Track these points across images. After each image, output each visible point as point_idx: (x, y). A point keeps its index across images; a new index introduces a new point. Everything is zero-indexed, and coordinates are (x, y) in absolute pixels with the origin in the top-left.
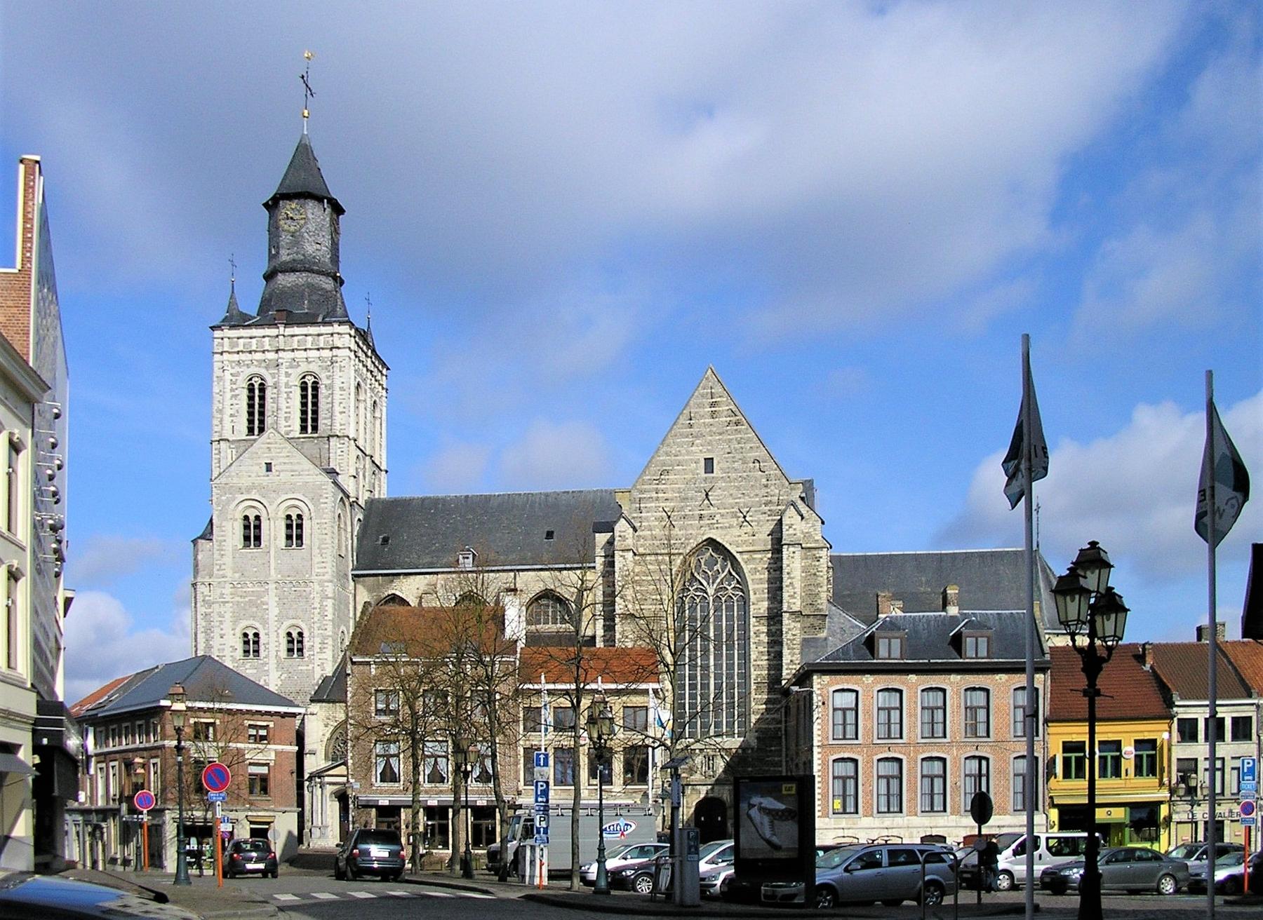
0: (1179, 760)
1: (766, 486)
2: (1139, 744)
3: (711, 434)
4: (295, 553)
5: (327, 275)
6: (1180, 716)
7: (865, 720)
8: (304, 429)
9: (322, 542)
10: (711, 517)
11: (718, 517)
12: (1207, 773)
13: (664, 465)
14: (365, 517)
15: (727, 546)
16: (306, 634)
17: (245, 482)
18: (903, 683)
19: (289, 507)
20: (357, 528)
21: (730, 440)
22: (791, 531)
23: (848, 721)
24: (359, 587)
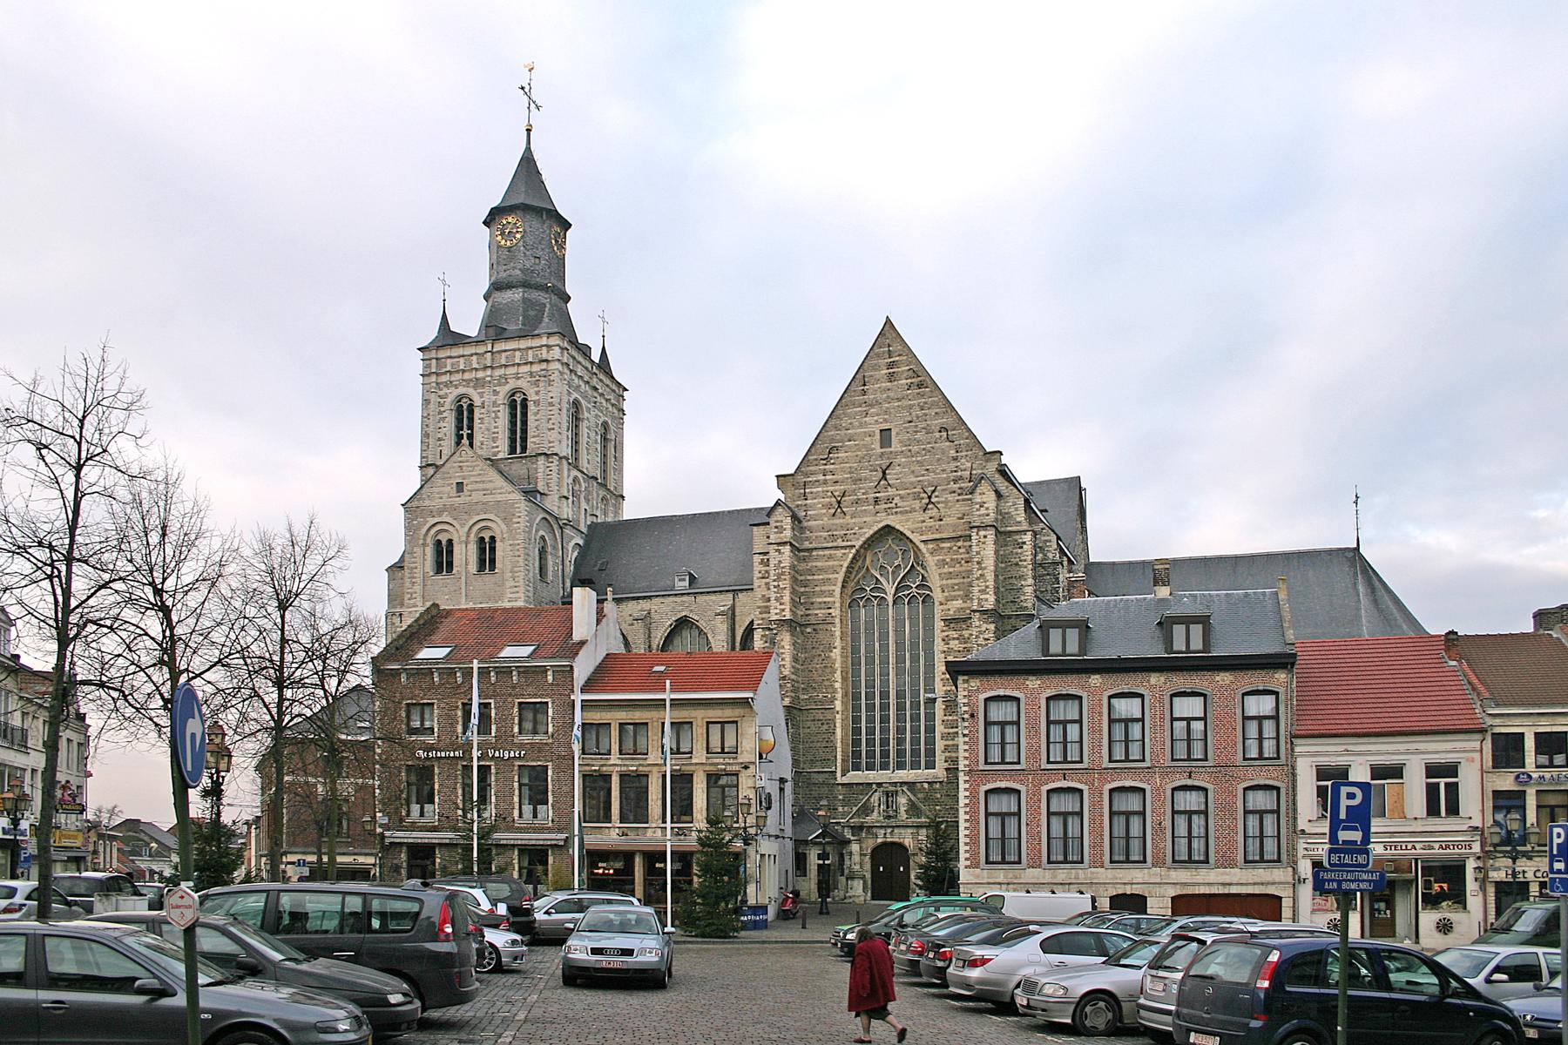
0: (1494, 792)
1: (955, 459)
2: (1433, 771)
3: (889, 400)
4: (488, 578)
5: (545, 288)
6: (1497, 730)
7: (1028, 737)
8: (513, 450)
9: (515, 564)
10: (889, 500)
11: (897, 500)
12: (577, 636)
13: (832, 440)
14: (587, 543)
15: (908, 533)
17: (437, 503)
18: (1083, 687)
19: (482, 529)
21: (911, 407)
22: (983, 511)
23: (1059, 747)
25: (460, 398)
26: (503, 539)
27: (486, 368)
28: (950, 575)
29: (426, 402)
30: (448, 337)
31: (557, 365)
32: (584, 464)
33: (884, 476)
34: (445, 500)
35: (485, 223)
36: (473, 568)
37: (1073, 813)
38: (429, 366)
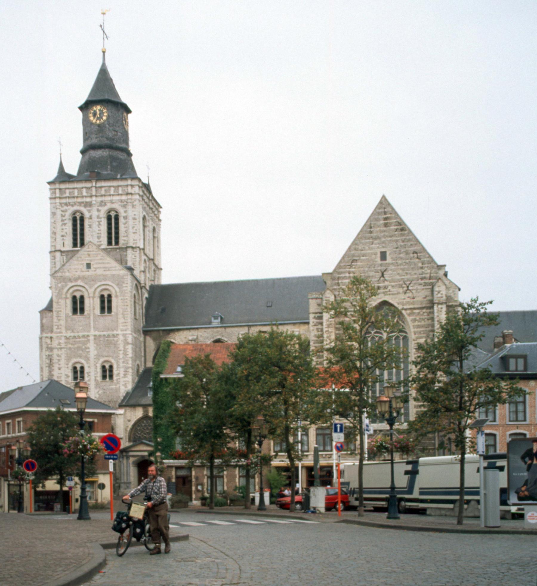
1: (422, 268)
3: (385, 236)
4: (107, 319)
10: (386, 287)
11: (390, 288)
15: (396, 305)
16: (115, 367)
19: (102, 290)
20: (145, 303)
22: (439, 295)
24: (148, 339)
25: (74, 213)
26: (117, 296)
27: (91, 196)
28: (418, 327)
29: (53, 214)
30: (63, 177)
31: (137, 197)
32: (147, 251)
33: (383, 275)
34: (79, 273)
35: (81, 108)
36: (98, 311)
37: (491, 445)
38: (55, 193)
